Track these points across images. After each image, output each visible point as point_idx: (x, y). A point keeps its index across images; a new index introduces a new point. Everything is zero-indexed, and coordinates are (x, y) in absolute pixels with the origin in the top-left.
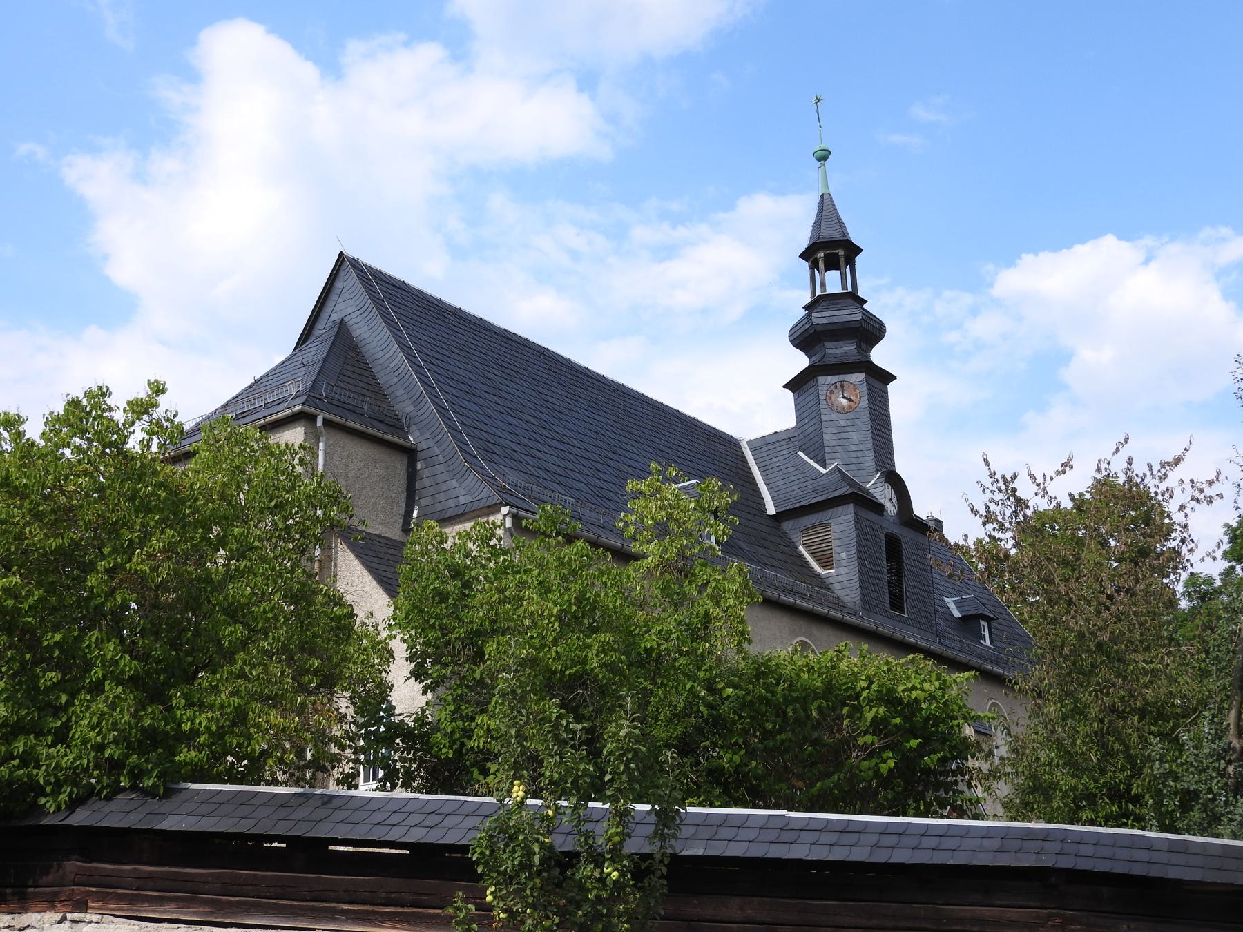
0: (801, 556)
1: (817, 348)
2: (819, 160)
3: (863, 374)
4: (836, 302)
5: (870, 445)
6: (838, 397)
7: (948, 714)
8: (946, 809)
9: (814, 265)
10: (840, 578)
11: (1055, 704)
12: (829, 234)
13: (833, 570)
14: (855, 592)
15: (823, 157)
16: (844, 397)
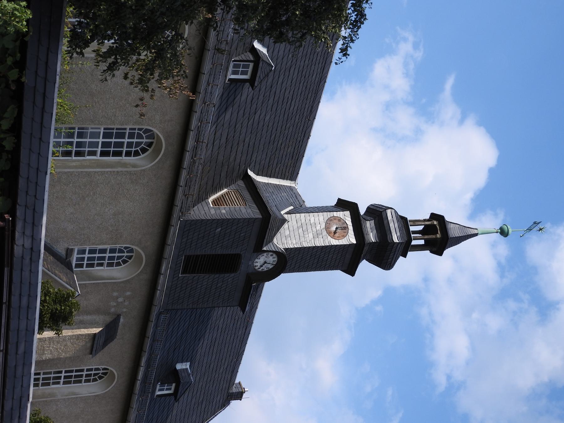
0: (221, 189)
3: (355, 242)
4: (404, 229)
5: (305, 245)
6: (336, 224)
10: (206, 208)
13: (212, 206)
14: (198, 217)
15: (503, 232)
16: (337, 228)
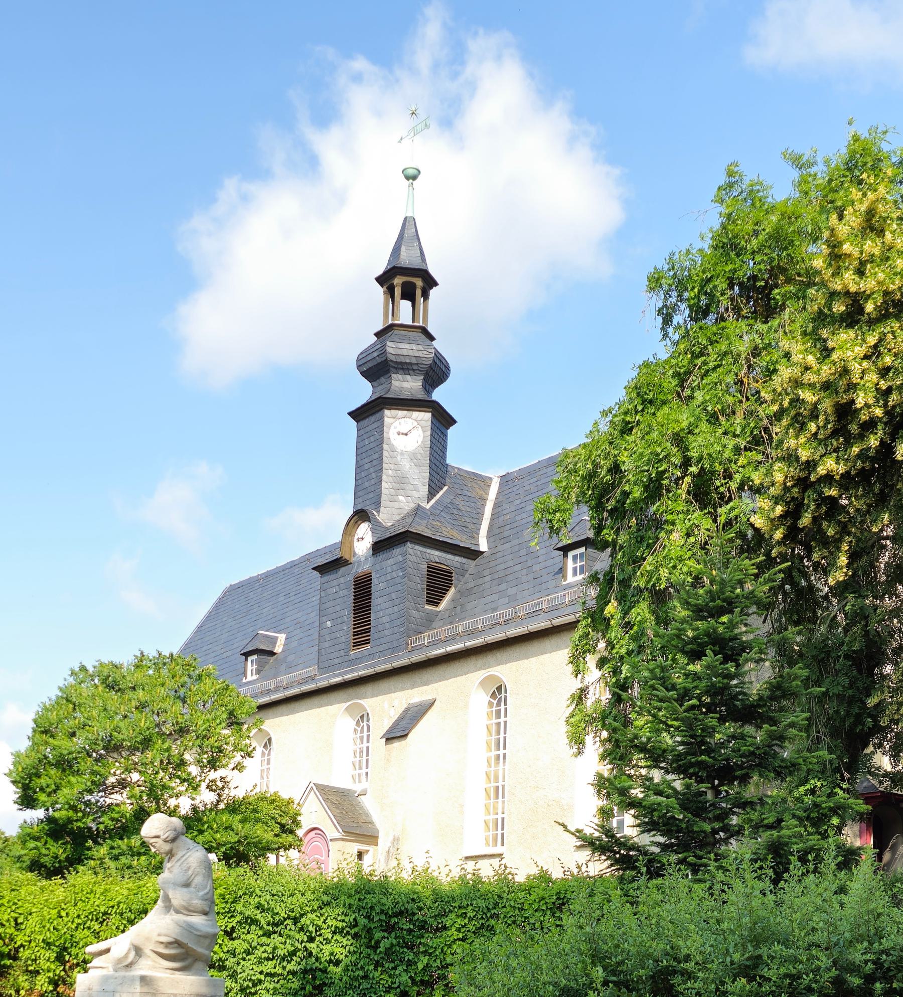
1: (382, 379)
2: (408, 178)
9: (390, 291)
11: (864, 385)
12: (407, 258)
15: (412, 177)
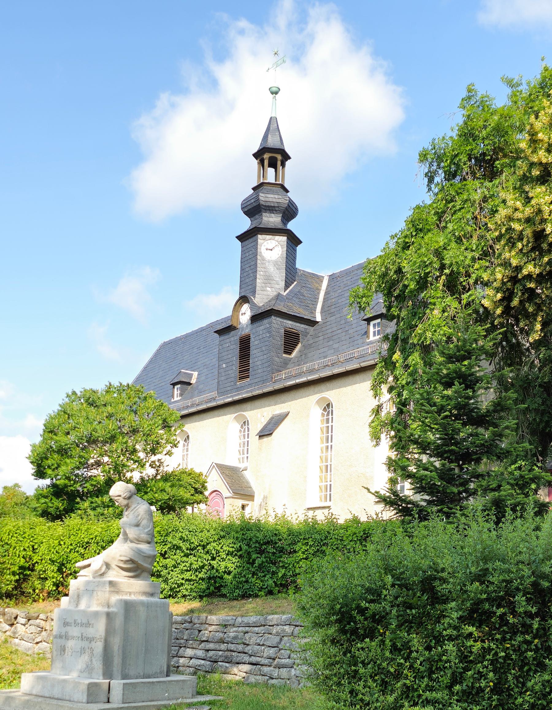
1: (257, 216)
7: (509, 367)
8: (104, 679)
9: (262, 162)
12: (272, 142)
15: (275, 92)
